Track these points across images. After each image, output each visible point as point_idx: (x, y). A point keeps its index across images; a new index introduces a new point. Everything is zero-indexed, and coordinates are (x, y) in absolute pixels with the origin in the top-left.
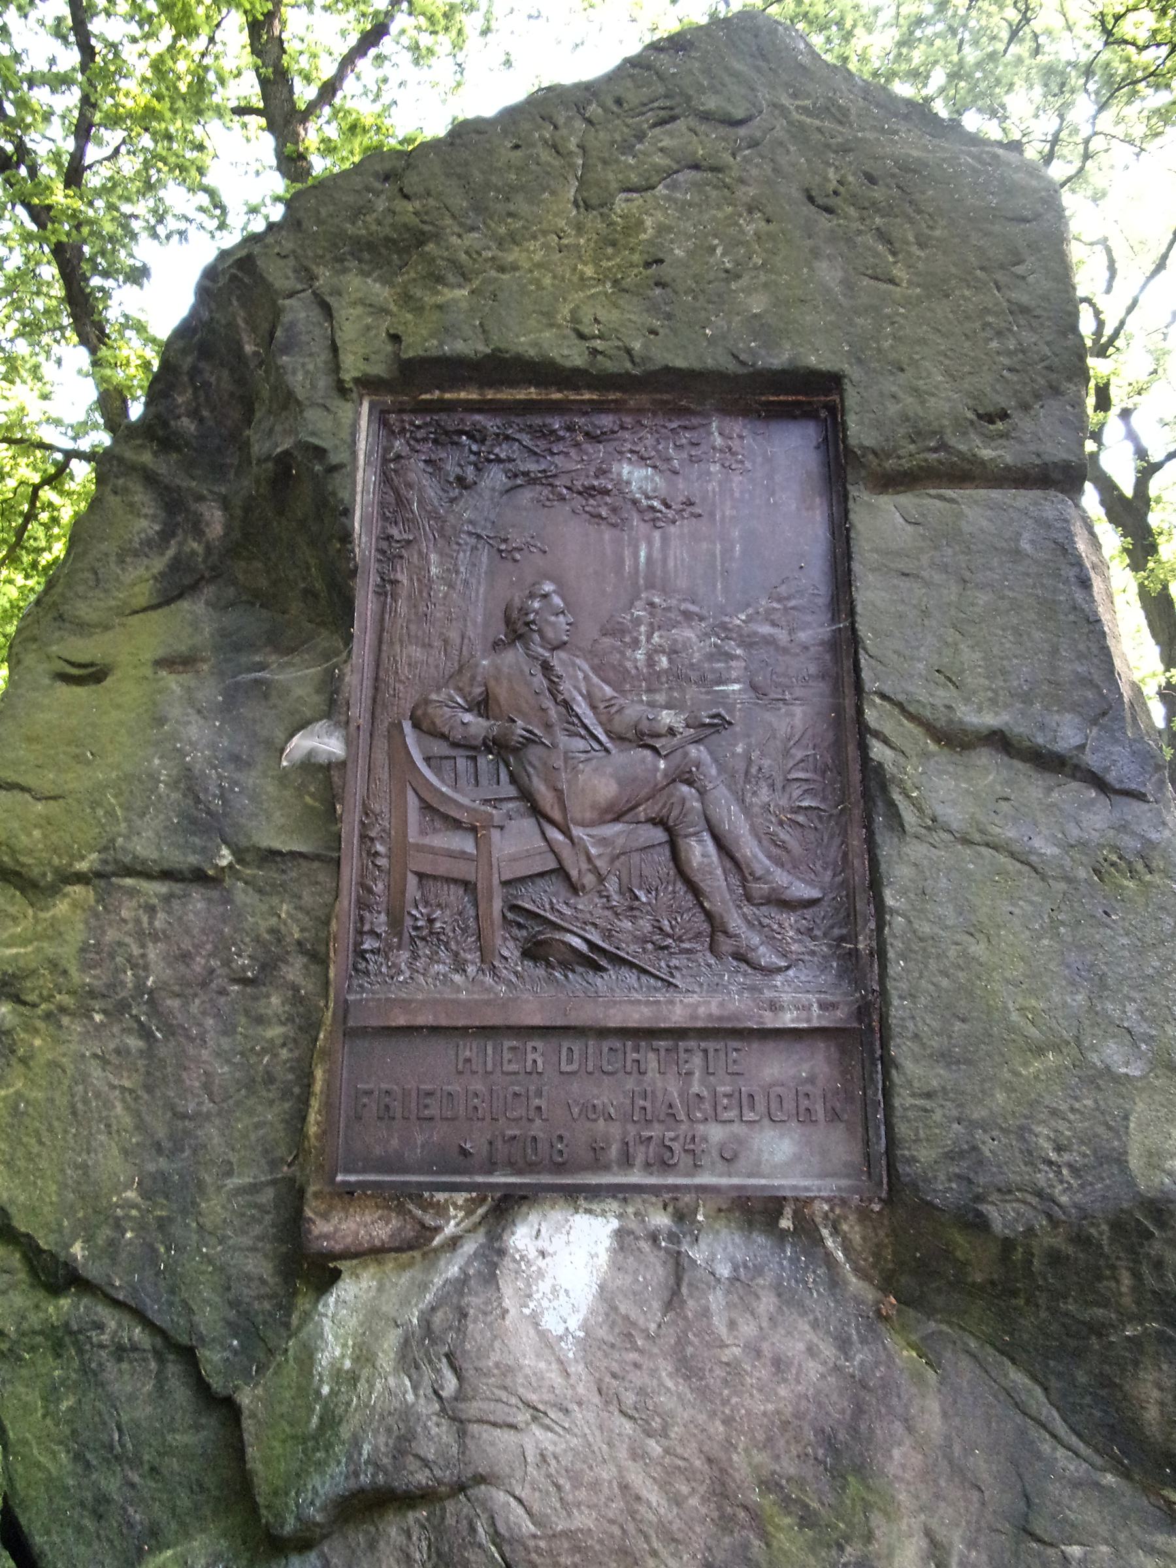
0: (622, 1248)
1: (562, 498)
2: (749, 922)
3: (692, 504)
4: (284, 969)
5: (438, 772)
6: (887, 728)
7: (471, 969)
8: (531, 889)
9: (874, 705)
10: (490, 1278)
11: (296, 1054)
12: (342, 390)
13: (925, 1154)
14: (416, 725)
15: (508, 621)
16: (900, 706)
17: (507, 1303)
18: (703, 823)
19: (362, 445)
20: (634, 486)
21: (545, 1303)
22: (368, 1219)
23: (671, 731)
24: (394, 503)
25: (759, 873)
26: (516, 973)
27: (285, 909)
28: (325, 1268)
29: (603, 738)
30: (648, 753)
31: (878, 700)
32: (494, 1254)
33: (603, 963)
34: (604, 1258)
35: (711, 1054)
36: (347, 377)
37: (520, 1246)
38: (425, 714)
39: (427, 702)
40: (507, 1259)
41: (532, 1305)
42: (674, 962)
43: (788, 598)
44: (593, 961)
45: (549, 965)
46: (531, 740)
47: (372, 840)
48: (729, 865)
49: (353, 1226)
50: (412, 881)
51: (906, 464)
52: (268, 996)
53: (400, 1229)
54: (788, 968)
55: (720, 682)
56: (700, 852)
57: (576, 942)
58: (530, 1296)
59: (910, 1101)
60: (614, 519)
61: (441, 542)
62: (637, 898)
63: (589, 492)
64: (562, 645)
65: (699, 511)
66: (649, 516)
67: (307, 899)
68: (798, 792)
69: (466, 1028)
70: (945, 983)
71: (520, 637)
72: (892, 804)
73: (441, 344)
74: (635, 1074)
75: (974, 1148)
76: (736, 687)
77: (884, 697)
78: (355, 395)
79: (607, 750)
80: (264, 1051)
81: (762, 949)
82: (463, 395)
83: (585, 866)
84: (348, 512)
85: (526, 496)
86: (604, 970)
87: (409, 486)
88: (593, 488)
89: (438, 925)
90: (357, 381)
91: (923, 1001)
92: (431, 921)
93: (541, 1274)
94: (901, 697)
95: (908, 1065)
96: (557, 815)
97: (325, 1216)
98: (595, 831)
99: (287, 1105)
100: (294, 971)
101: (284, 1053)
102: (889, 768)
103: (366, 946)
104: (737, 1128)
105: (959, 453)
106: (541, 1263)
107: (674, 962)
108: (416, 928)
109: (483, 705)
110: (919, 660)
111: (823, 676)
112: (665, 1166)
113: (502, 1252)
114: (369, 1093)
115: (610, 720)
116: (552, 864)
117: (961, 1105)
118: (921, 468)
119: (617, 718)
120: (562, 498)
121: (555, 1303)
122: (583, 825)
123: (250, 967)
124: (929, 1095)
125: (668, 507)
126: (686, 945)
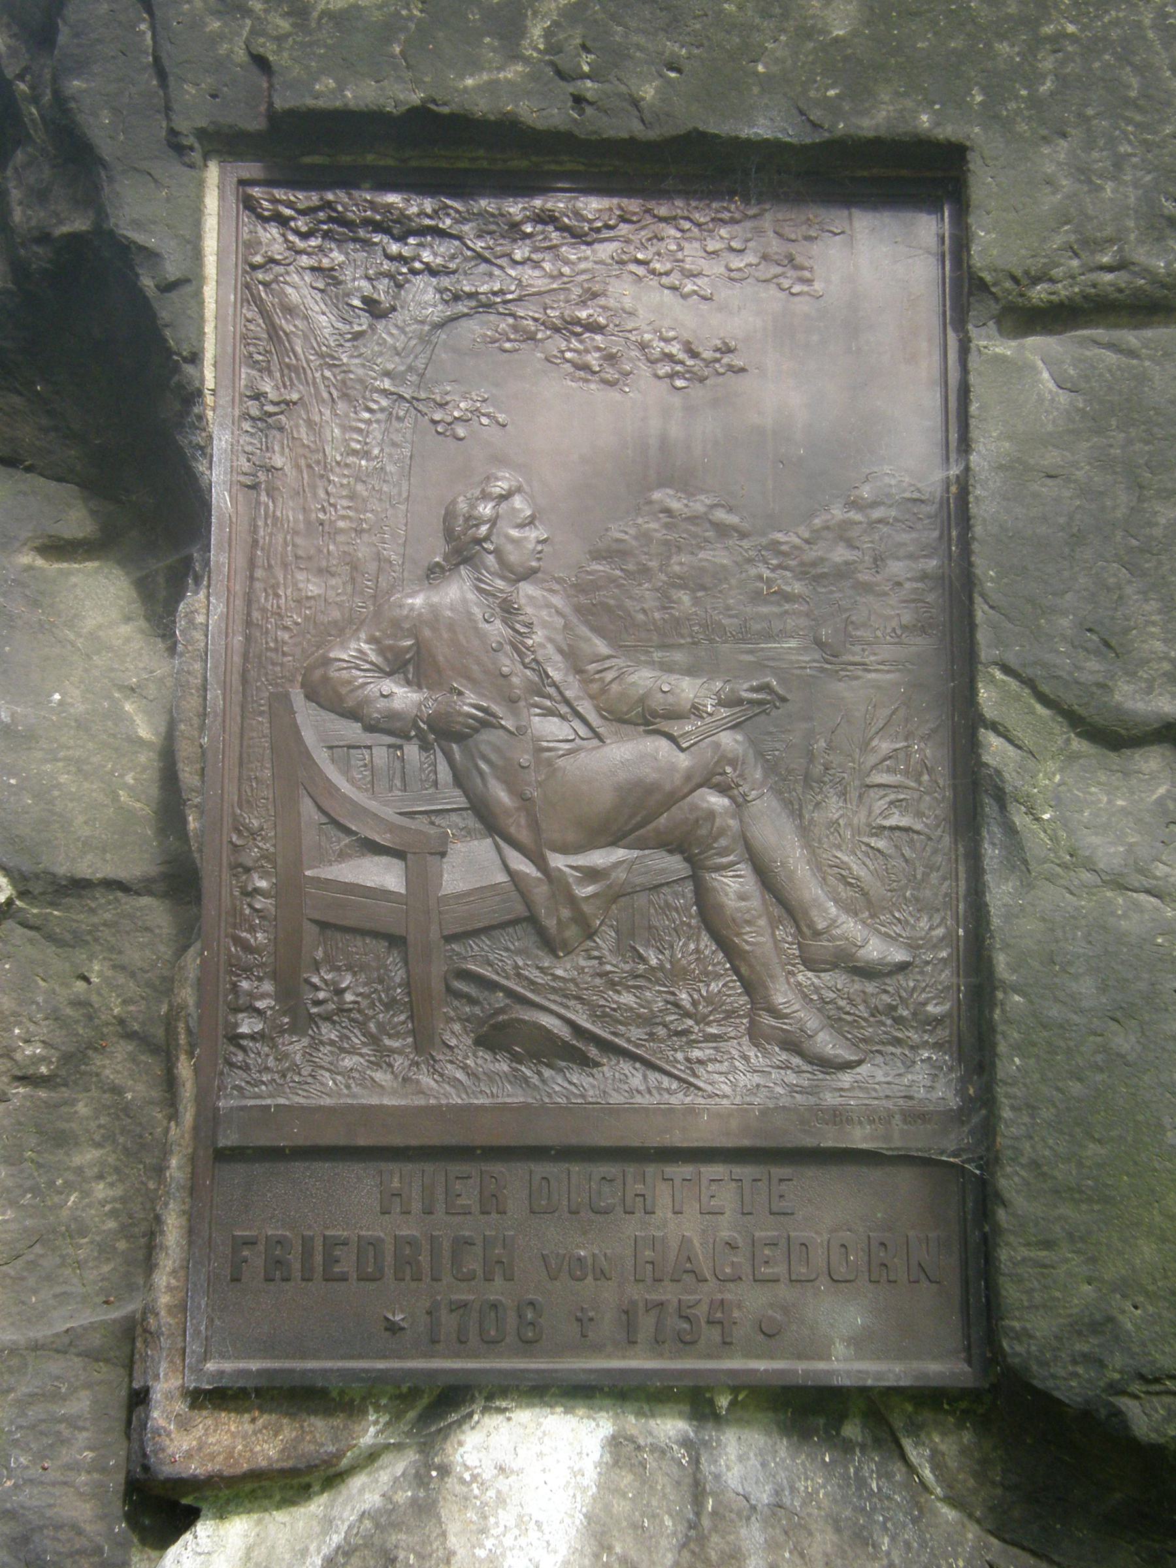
0: (616, 1463)
1: (531, 337)
2: (805, 996)
3: (730, 351)
4: (98, 1060)
5: (346, 771)
6: (1011, 718)
7: (399, 1062)
8: (476, 946)
9: (992, 680)
10: (425, 1509)
11: (118, 1191)
12: (176, 146)
13: (1042, 1326)
14: (311, 696)
15: (449, 534)
16: (1029, 683)
17: (453, 1541)
18: (740, 849)
19: (210, 244)
20: (640, 322)
21: (508, 1541)
22: (249, 1428)
23: (696, 711)
24: (268, 335)
25: (821, 925)
26: (465, 1068)
27: (96, 969)
28: (175, 1504)
29: (593, 718)
30: (664, 744)
31: (999, 675)
32: (431, 1474)
33: (593, 1052)
34: (591, 1475)
35: (747, 1185)
36: (183, 125)
37: (471, 1460)
38: (326, 679)
39: (327, 662)
40: (451, 1481)
41: (489, 1543)
42: (696, 1054)
43: (874, 504)
44: (577, 1051)
45: (516, 1058)
46: (488, 722)
47: (248, 870)
48: (777, 911)
49: (226, 1439)
50: (311, 930)
51: (1063, 291)
52: (72, 1102)
53: (298, 1440)
54: (860, 1063)
55: (769, 636)
56: (734, 886)
57: (547, 1021)
58: (483, 1531)
59: (1024, 1252)
60: (611, 374)
61: (341, 406)
62: (643, 959)
63: (569, 327)
64: (528, 575)
65: (739, 363)
66: (664, 369)
67: (134, 956)
68: (882, 804)
69: (407, 1149)
70: (1076, 1088)
71: (466, 561)
72: (1011, 830)
73: (341, 88)
74: (639, 1214)
75: (1110, 1319)
76: (793, 644)
77: (1006, 669)
78: (196, 156)
79: (598, 736)
80: (69, 1186)
81: (823, 1037)
82: (370, 158)
83: (566, 913)
84: (195, 358)
85: (475, 329)
86: (597, 1064)
87: (289, 310)
88: (578, 322)
89: (349, 997)
90: (201, 134)
91: (1046, 1113)
92: (340, 992)
93: (501, 1500)
94: (1029, 672)
95: (1020, 1202)
96: (524, 836)
97: (184, 1425)
98: (581, 860)
99: (106, 1269)
100: (116, 1065)
101: (100, 1190)
102: (1012, 779)
103: (244, 1029)
104: (784, 1292)
105: (1146, 272)
106: (502, 1484)
107: (696, 1054)
108: (317, 1003)
109: (410, 663)
110: (1064, 613)
111: (921, 628)
112: (686, 1343)
113: (445, 1470)
114: (250, 1243)
115: (604, 691)
116: (520, 910)
117: (1093, 1260)
118: (1086, 297)
119: (615, 687)
120: (531, 337)
121: (522, 1541)
122: (565, 850)
123: (43, 1059)
124: (1048, 1244)
125: (694, 355)
126: (713, 1030)
